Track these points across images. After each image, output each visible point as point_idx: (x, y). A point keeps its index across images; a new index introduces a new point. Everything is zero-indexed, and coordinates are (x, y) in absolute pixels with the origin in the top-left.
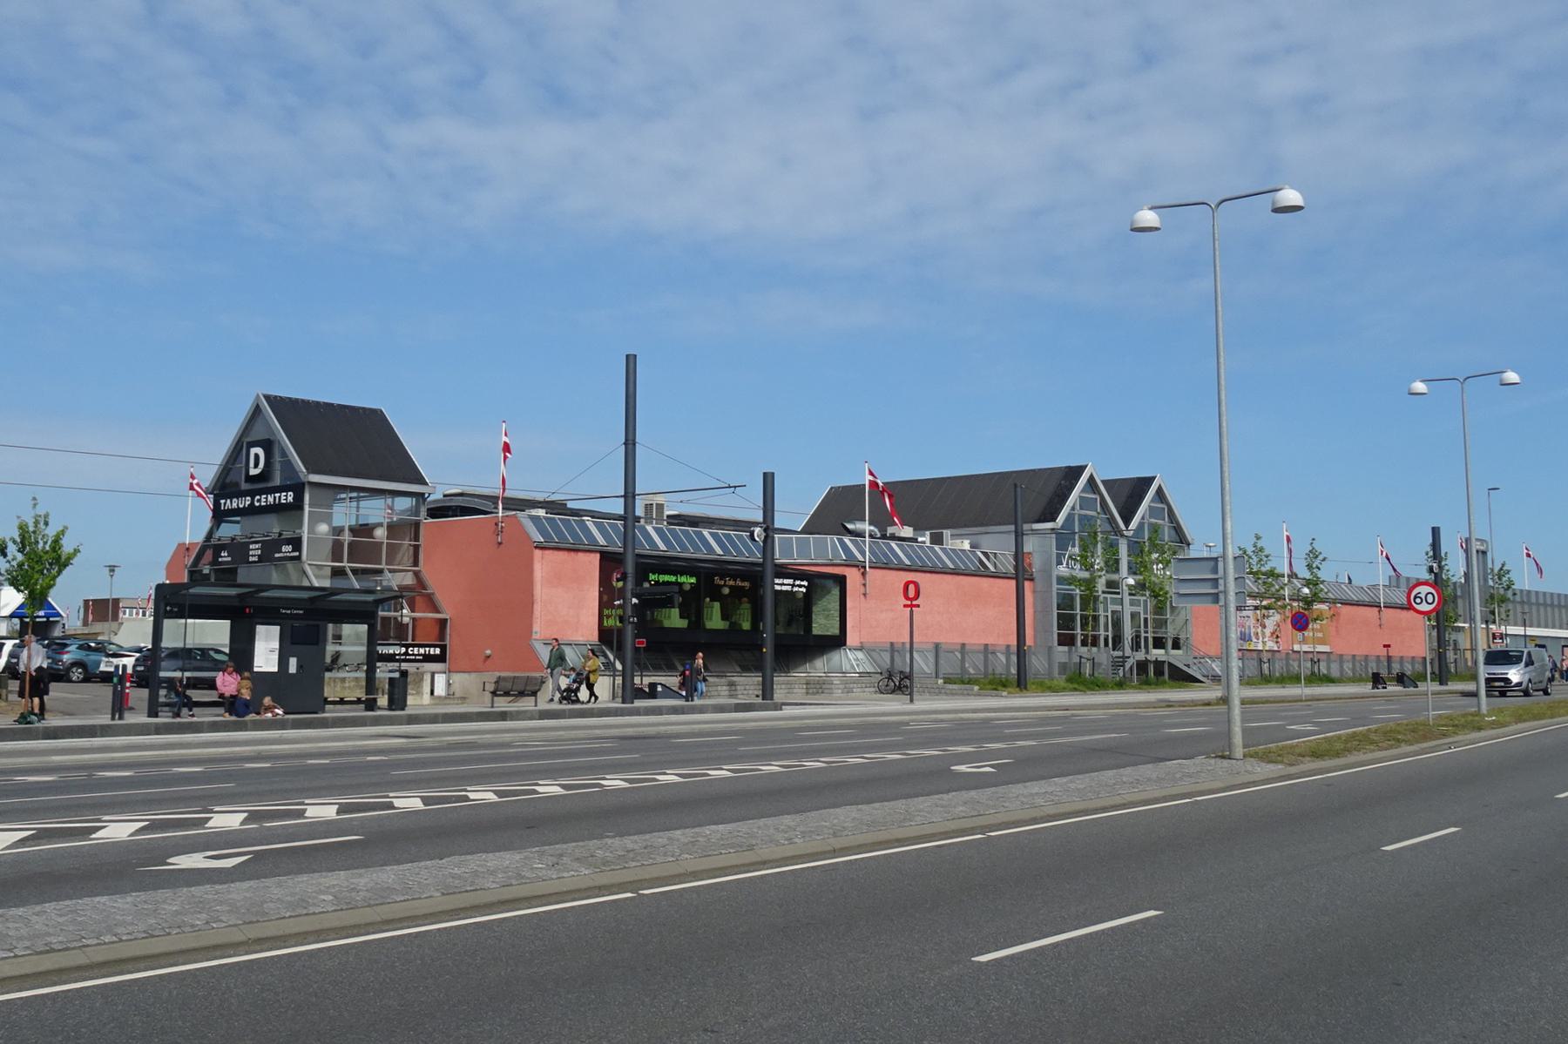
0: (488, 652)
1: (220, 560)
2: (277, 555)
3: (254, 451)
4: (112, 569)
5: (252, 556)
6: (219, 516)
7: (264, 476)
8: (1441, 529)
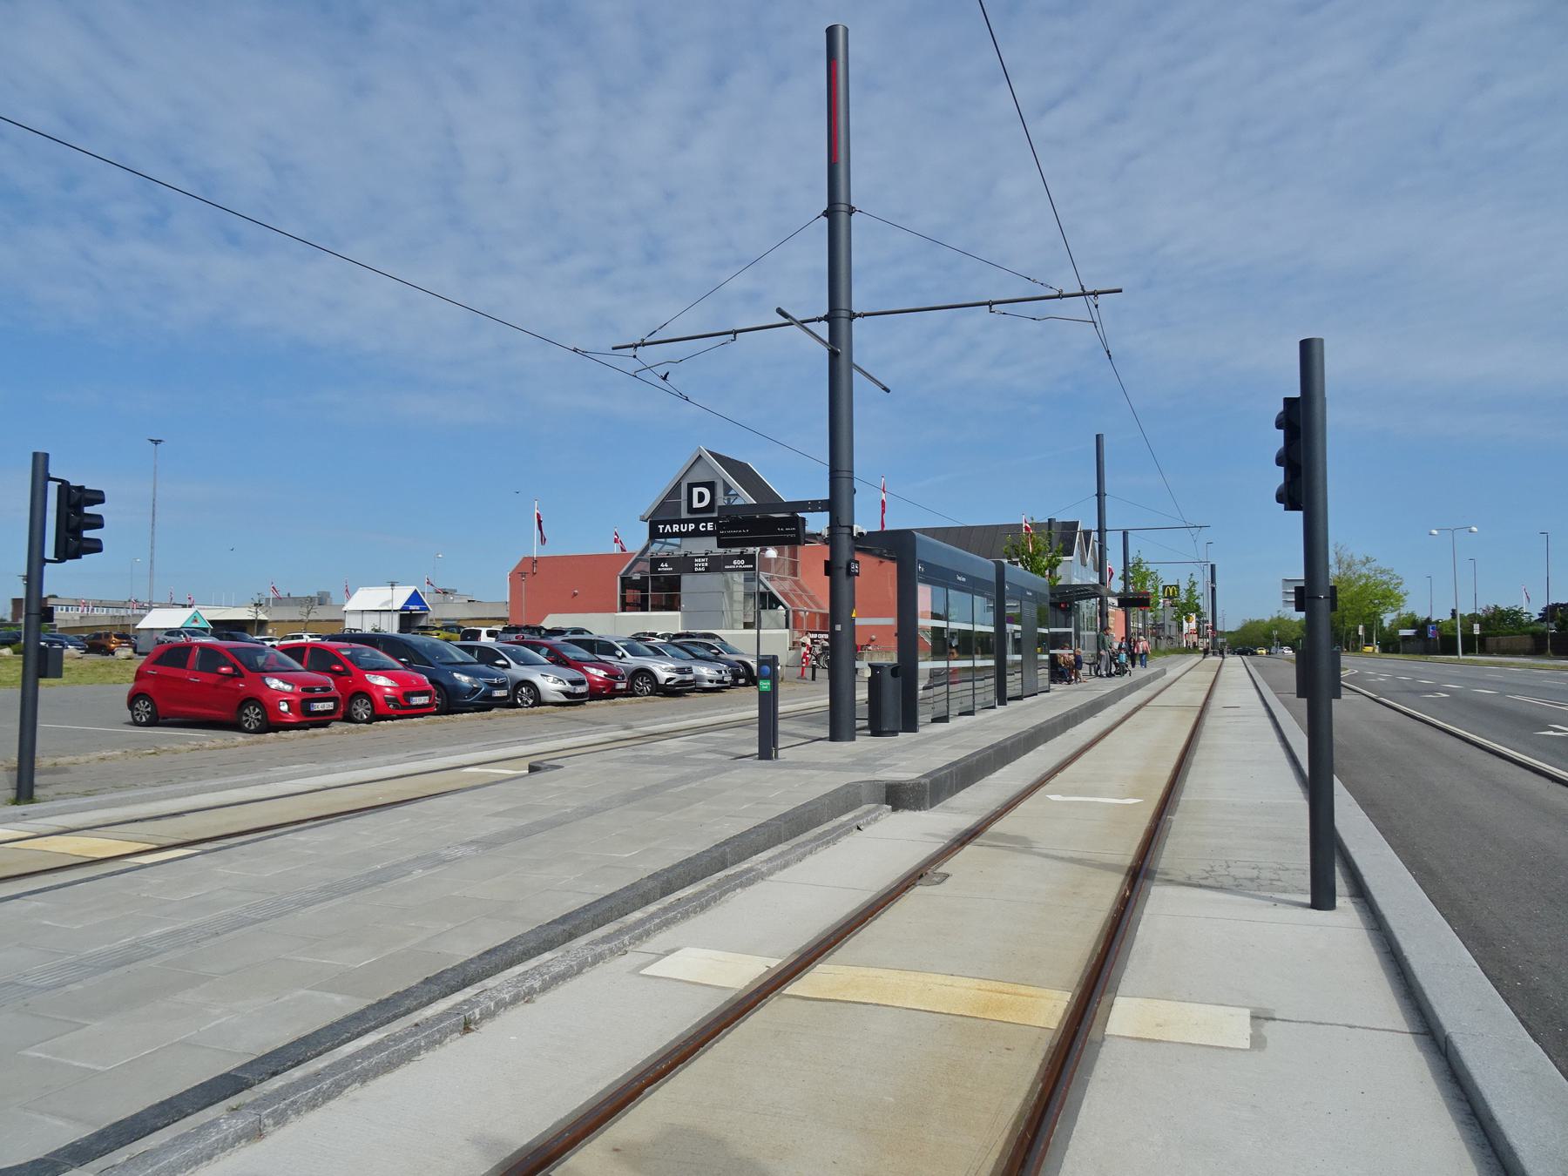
0: (874, 637)
3: (696, 491)
6: (654, 534)
8: (50, 457)
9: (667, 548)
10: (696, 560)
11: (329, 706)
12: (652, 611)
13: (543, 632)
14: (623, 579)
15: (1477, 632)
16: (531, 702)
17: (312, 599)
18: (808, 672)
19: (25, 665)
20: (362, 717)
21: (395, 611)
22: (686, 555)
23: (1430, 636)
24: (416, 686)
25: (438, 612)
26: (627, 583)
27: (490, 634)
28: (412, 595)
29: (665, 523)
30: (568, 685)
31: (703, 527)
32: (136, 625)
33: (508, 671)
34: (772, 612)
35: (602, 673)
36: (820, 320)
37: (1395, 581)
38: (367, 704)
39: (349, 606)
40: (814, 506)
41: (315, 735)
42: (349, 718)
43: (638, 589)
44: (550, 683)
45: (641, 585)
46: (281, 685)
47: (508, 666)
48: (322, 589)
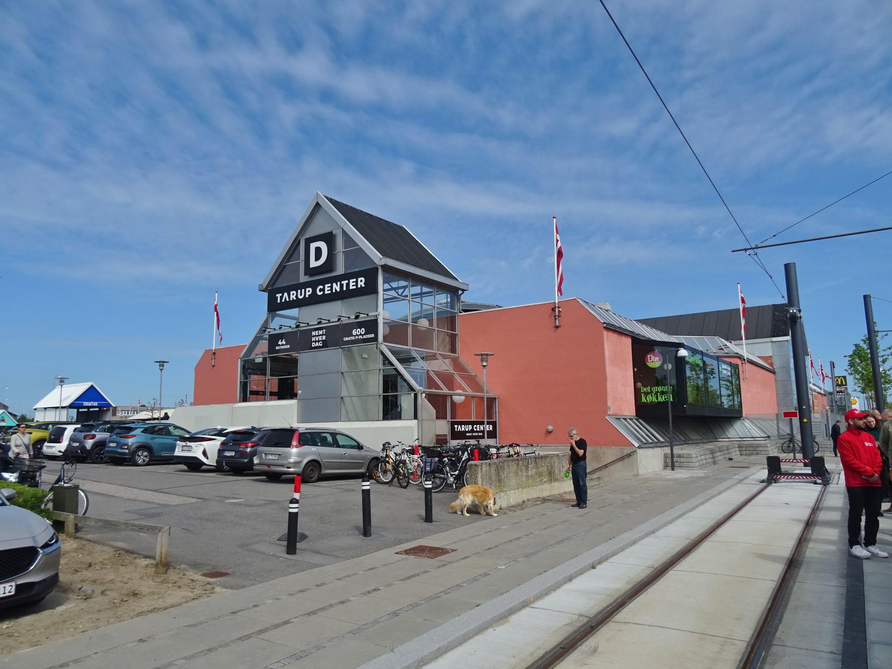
0: (550, 428)
1: (277, 348)
2: (346, 339)
4: (162, 363)
5: (315, 342)
6: (274, 307)
7: (329, 265)
10: (314, 333)
19: (812, 433)
31: (320, 290)
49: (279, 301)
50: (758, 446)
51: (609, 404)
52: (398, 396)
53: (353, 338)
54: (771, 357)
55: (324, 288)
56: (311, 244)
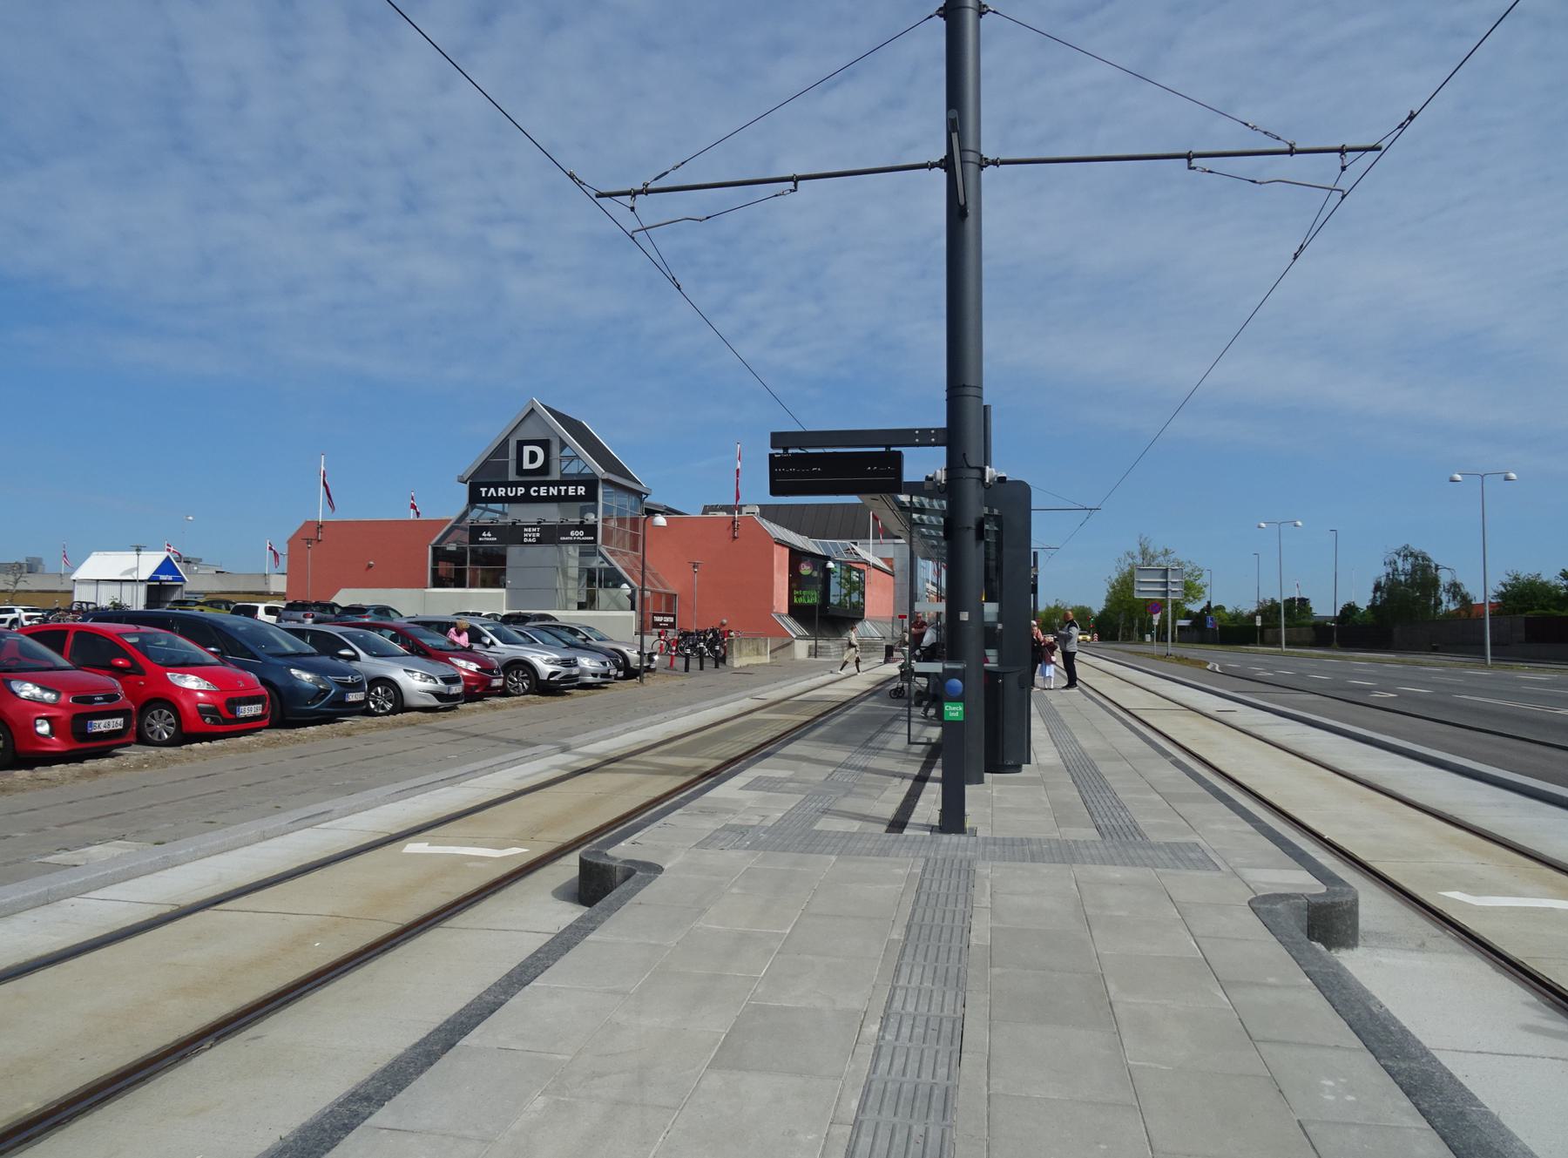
0: (725, 621)
1: (480, 539)
3: (527, 449)
6: (475, 498)
9: (488, 515)
10: (526, 530)
11: (116, 723)
12: (470, 587)
13: (337, 611)
14: (435, 549)
15: (1259, 624)
16: (389, 706)
17: (21, 566)
18: (680, 662)
20: (160, 736)
21: (140, 581)
22: (514, 523)
23: (1209, 626)
24: (241, 689)
25: (197, 582)
26: (439, 554)
27: (269, 611)
28: (802, 505)
29: (488, 486)
30: (440, 683)
31: (535, 491)
32: (72, 574)
33: (355, 665)
34: (614, 591)
35: (473, 667)
36: (931, 166)
37: (1197, 573)
38: (169, 717)
39: (77, 575)
40: (922, 438)
41: (97, 772)
42: (143, 740)
43: (451, 562)
44: (414, 681)
45: (457, 557)
46: (37, 691)
47: (356, 658)
48: (32, 555)
49: (483, 495)
50: (876, 644)
51: (775, 604)
52: (1165, 644)
53: (571, 538)
54: (892, 559)
55: (539, 489)
56: (525, 447)
